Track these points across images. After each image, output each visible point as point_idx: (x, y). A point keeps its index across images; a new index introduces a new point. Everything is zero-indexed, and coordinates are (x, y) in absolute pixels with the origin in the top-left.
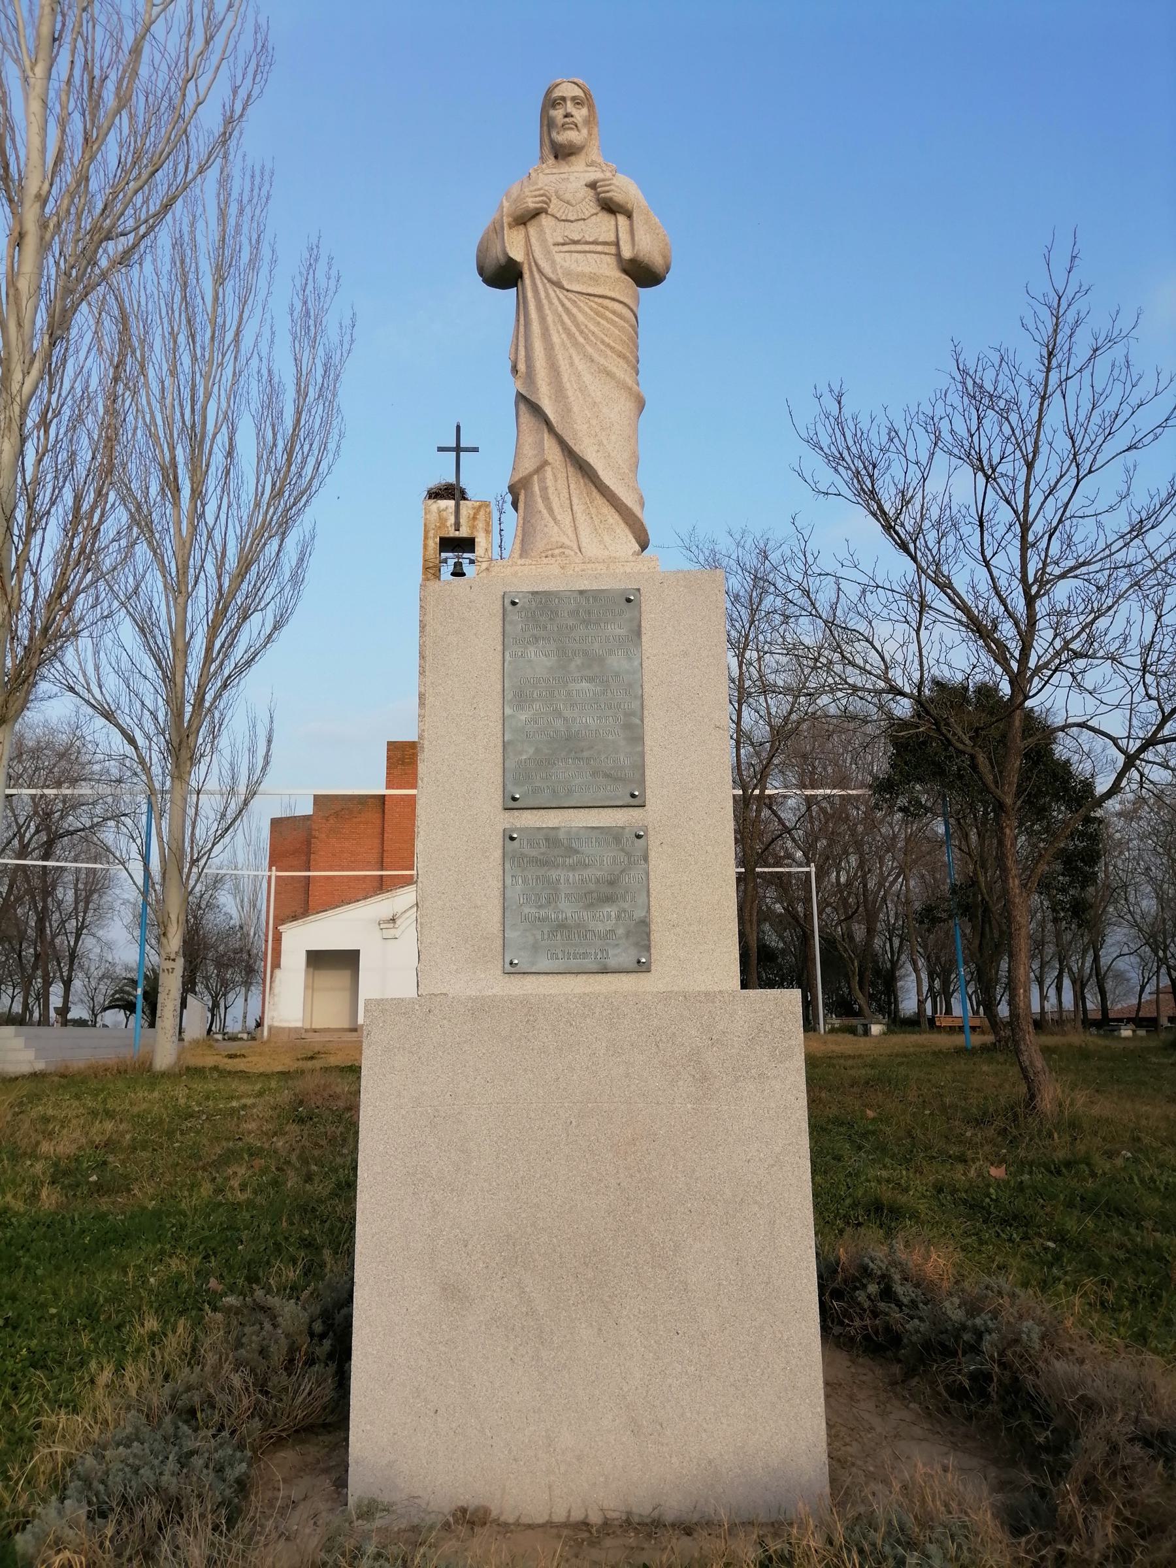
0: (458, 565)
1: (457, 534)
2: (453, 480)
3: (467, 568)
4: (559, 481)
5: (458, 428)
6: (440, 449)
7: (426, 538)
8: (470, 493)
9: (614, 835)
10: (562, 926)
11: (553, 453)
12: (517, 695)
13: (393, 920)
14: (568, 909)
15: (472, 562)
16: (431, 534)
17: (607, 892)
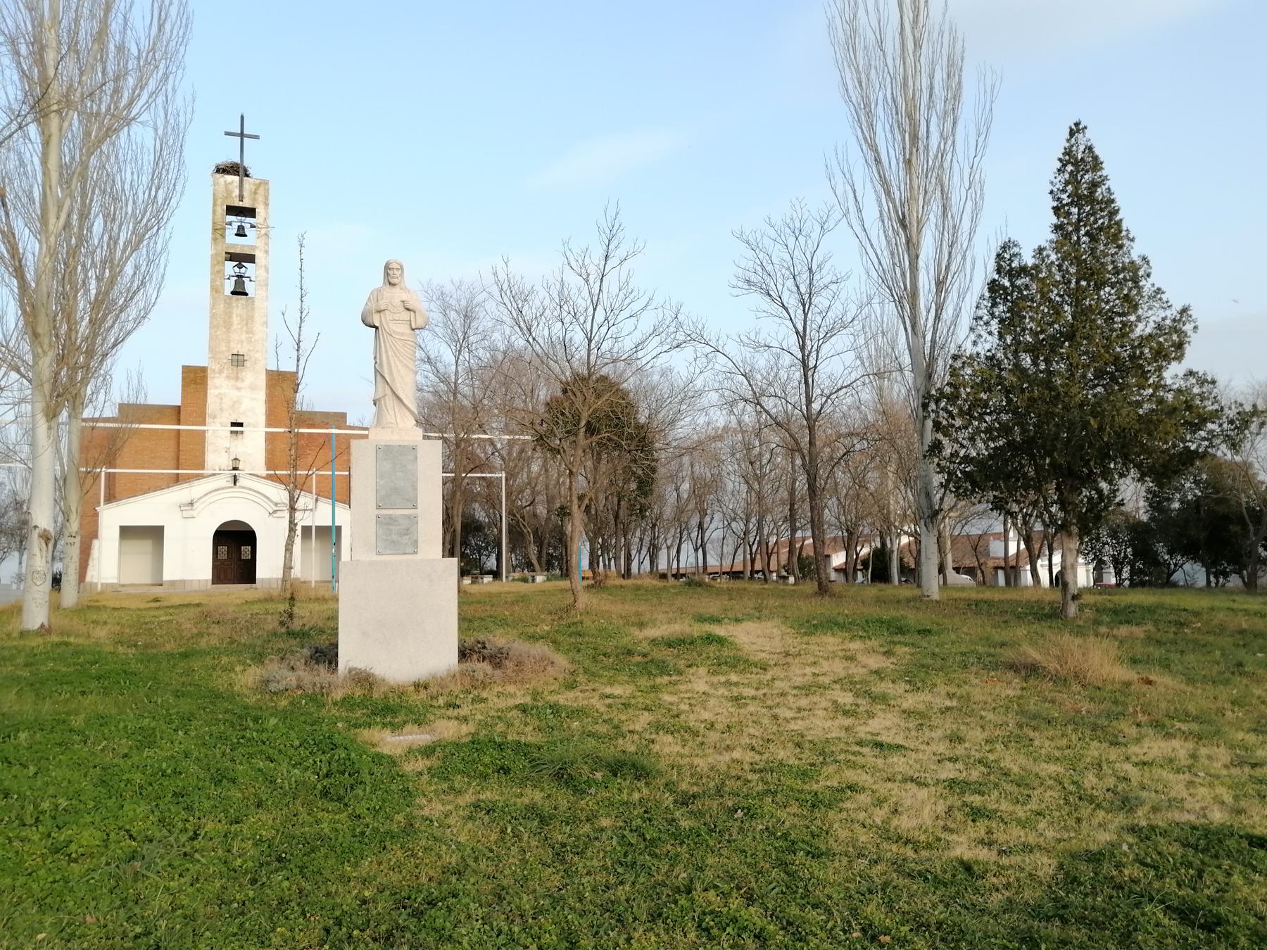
0: (241, 228)
1: (241, 204)
2: (237, 160)
3: (248, 231)
4: (390, 401)
5: (242, 117)
6: (227, 134)
7: (215, 205)
8: (250, 171)
9: (408, 517)
10: (393, 542)
11: (388, 392)
12: (380, 475)
13: (191, 504)
14: (395, 537)
15: (253, 226)
16: (219, 202)
17: (407, 532)
